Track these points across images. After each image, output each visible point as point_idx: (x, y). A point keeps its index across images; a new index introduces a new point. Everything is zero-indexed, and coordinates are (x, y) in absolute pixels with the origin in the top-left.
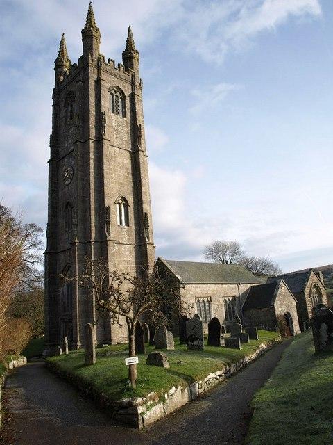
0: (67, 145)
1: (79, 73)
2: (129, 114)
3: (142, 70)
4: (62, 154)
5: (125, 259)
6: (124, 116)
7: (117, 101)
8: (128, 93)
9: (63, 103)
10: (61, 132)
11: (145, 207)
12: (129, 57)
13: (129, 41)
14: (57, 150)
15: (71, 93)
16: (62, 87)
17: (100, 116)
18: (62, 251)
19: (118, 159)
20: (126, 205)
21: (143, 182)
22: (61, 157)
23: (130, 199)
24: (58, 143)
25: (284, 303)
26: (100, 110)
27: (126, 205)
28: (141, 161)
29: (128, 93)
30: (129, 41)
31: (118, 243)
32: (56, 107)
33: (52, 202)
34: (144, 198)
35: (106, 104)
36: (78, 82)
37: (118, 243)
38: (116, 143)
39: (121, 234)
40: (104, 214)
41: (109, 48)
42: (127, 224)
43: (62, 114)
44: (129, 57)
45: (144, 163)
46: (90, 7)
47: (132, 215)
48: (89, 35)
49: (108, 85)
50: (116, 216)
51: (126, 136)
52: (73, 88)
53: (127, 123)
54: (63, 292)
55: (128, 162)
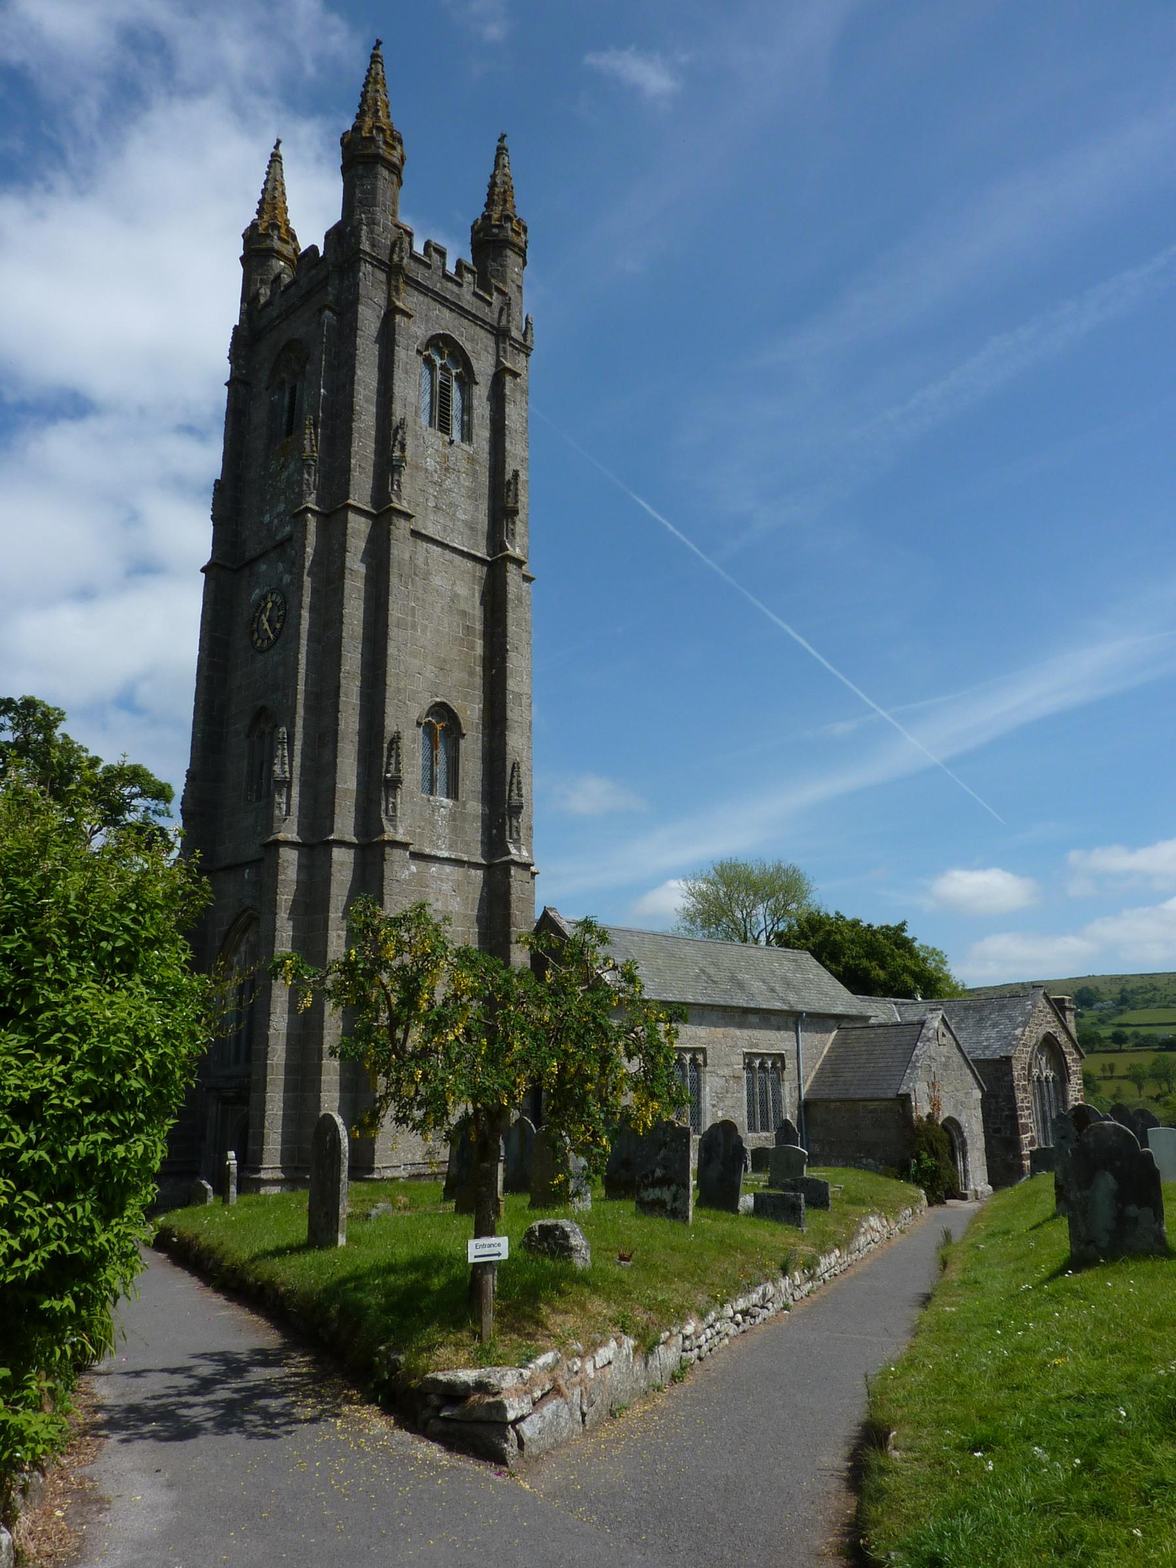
23: (471, 712)
29: (483, 367)
43: (259, 415)
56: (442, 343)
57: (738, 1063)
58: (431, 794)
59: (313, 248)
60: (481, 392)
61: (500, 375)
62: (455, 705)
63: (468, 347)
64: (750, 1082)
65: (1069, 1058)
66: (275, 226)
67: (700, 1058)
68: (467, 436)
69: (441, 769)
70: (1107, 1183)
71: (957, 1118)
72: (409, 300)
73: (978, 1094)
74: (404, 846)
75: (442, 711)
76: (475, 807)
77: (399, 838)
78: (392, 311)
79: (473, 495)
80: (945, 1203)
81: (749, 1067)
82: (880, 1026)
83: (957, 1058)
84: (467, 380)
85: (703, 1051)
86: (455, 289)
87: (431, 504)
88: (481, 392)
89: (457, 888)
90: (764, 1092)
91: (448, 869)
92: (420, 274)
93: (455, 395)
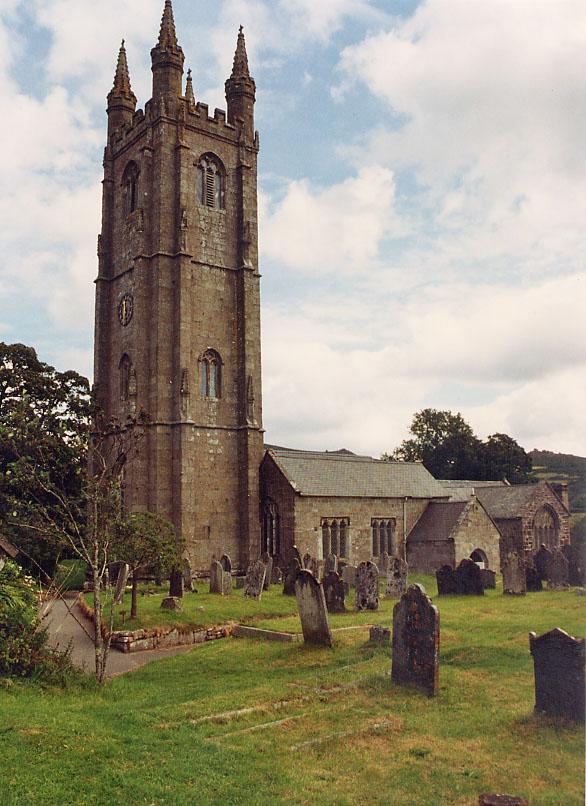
0: (129, 334)
1: (144, 133)
2: (230, 202)
3: (264, 113)
5: (211, 451)
6: (223, 205)
7: (210, 180)
8: (230, 165)
9: (119, 178)
11: (250, 366)
12: (240, 88)
15: (132, 163)
16: (118, 149)
17: (178, 211)
20: (218, 362)
22: (116, 275)
23: (225, 352)
26: (242, 370)
27: (218, 362)
29: (230, 165)
32: (109, 185)
33: (100, 372)
35: (190, 188)
36: (142, 150)
40: (177, 375)
42: (219, 395)
43: (118, 199)
44: (240, 88)
47: (227, 379)
48: (167, 58)
49: (196, 153)
50: (199, 381)
53: (226, 218)
56: (209, 156)
58: (79, 605)
59: (141, 110)
61: (240, 168)
62: (218, 349)
66: (123, 93)
71: (482, 548)
72: (188, 139)
73: (498, 537)
77: (189, 421)
78: (177, 148)
79: (225, 237)
80: (482, 594)
82: (454, 503)
83: (485, 519)
86: (214, 126)
87: (204, 245)
90: (382, 536)
92: (193, 122)
93: (216, 183)
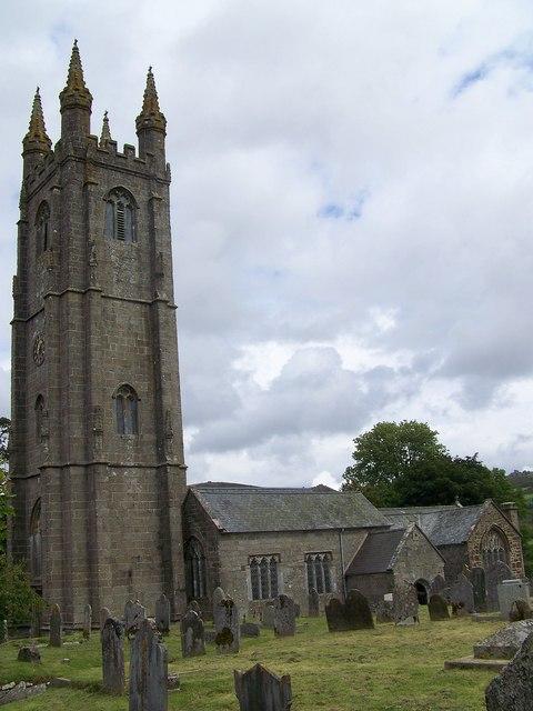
4: (33, 311)
5: (130, 491)
10: (31, 270)
11: (167, 400)
12: (151, 124)
13: (151, 96)
14: (25, 302)
18: (32, 477)
19: (118, 320)
21: (165, 357)
23: (142, 387)
24: (25, 291)
25: (450, 609)
28: (162, 319)
29: (141, 198)
30: (151, 96)
31: (117, 466)
34: (166, 385)
37: (117, 466)
38: (116, 291)
39: (124, 449)
40: (90, 413)
41: (115, 118)
43: (32, 239)
44: (151, 124)
45: (167, 322)
46: (75, 50)
48: (76, 101)
51: (135, 276)
52: (46, 195)
54: (35, 543)
55: (298, 528)
57: (301, 560)
60: (142, 213)
62: (133, 384)
63: (131, 190)
64: (309, 568)
65: (510, 538)
67: (277, 559)
68: (135, 238)
69: (128, 420)
70: (190, 630)
74: (106, 464)
75: (127, 388)
76: (149, 437)
81: (309, 561)
84: (133, 206)
85: (330, 553)
88: (142, 213)
89: (140, 480)
90: (319, 573)
91: (134, 471)
